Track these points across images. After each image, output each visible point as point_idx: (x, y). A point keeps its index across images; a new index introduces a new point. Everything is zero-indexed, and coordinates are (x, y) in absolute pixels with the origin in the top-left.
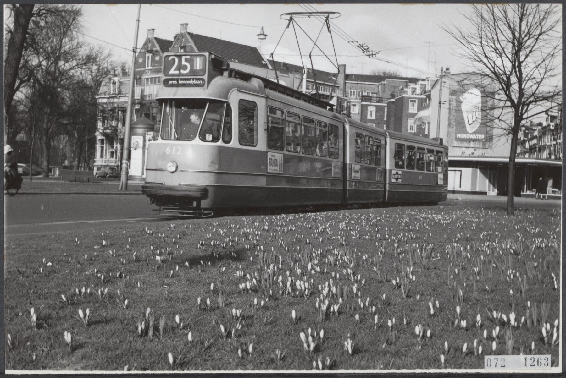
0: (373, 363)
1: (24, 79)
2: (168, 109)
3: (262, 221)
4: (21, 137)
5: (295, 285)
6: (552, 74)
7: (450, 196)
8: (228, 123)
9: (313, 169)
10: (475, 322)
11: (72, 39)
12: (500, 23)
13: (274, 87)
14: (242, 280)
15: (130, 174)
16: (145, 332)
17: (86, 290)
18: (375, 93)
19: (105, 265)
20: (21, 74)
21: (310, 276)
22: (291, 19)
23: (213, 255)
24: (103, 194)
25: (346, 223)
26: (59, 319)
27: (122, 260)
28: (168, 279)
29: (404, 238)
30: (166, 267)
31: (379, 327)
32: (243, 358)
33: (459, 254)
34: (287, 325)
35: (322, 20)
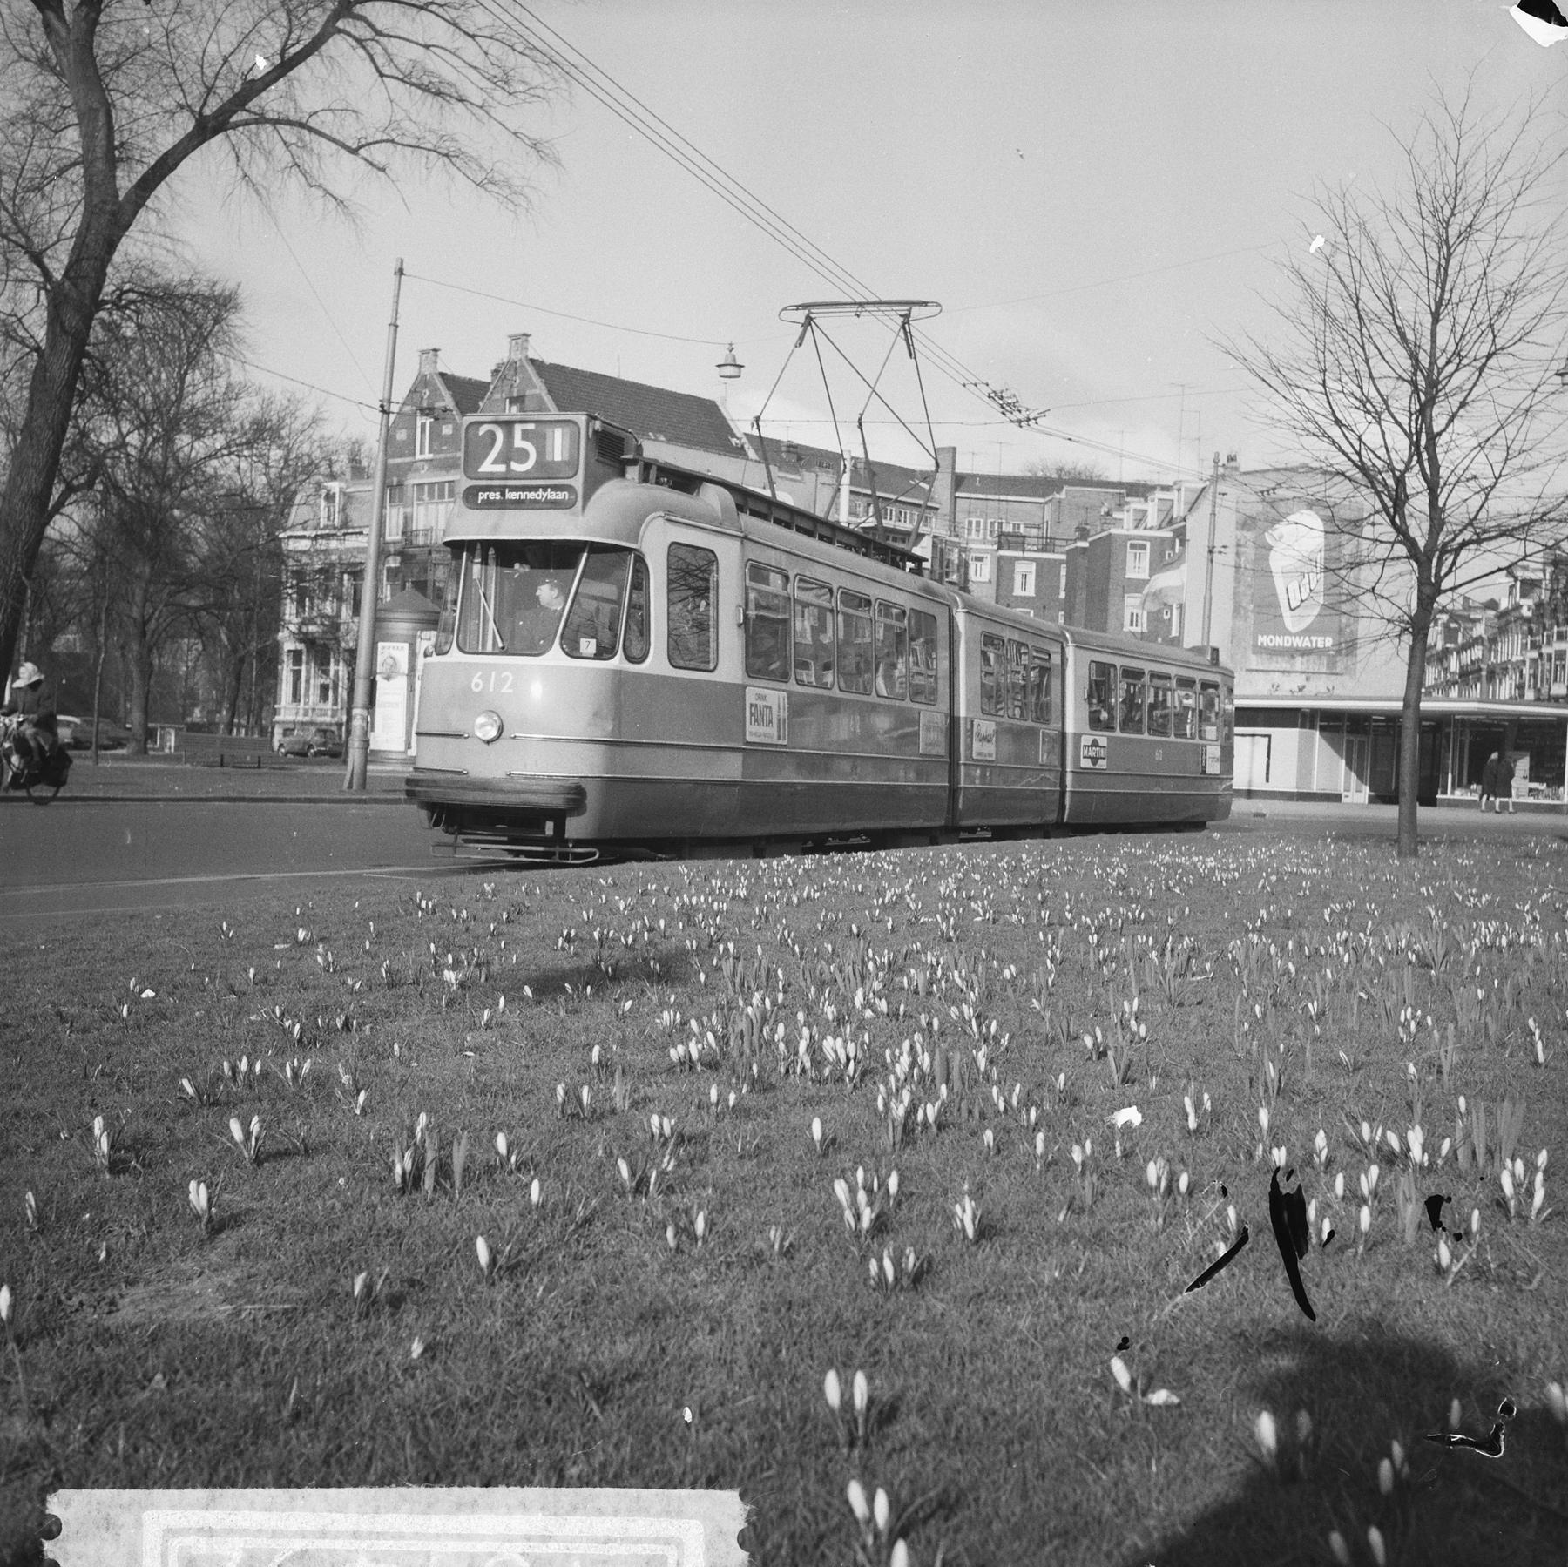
0: (1032, 1263)
1: (75, 482)
2: (476, 568)
3: (732, 874)
4: (68, 640)
5: (821, 1049)
6: (1527, 464)
7: (1239, 806)
8: (640, 608)
9: (868, 734)
10: (1311, 1152)
11: (211, 376)
12: (1374, 329)
13: (763, 508)
14: (676, 1037)
15: (372, 747)
16: (414, 1180)
17: (251, 1065)
18: (1034, 527)
19: (304, 995)
20: (68, 466)
21: (861, 1026)
22: (809, 320)
23: (598, 967)
24: (298, 800)
25: (957, 880)
26: (174, 1146)
27: (350, 982)
28: (476, 1034)
29: (1116, 921)
30: (471, 1001)
31: (1048, 1165)
32: (679, 1250)
33: (1264, 964)
34: (800, 1158)
35: (889, 323)
